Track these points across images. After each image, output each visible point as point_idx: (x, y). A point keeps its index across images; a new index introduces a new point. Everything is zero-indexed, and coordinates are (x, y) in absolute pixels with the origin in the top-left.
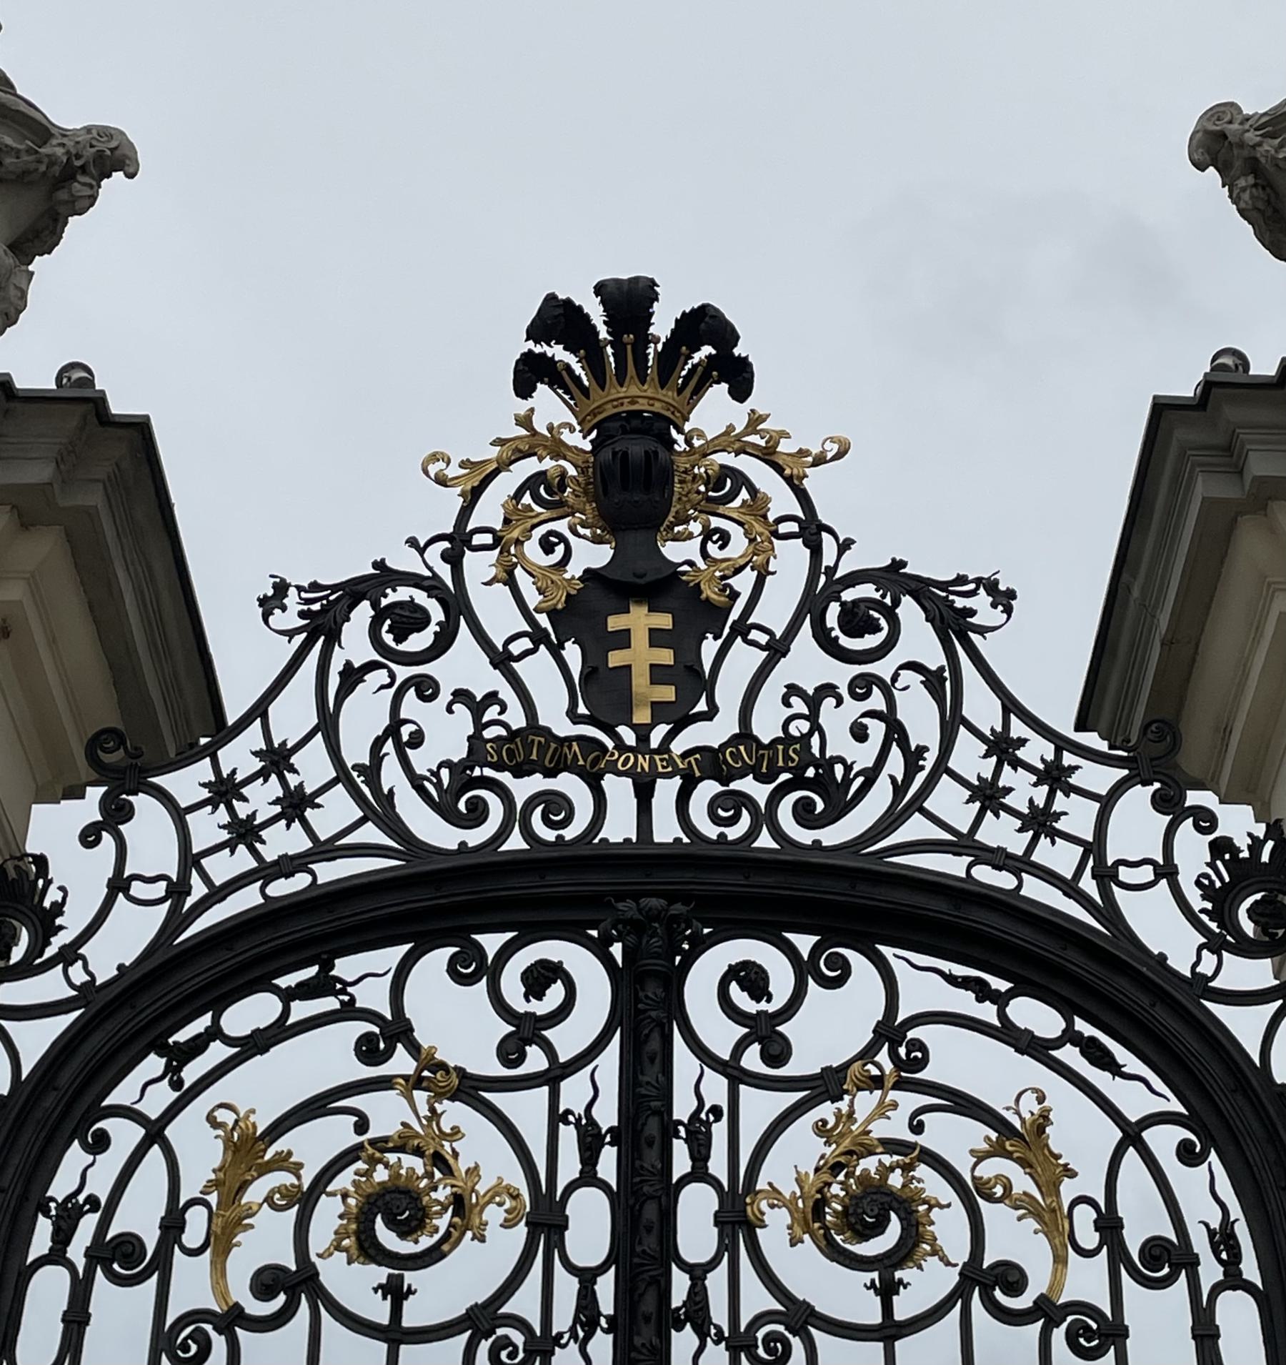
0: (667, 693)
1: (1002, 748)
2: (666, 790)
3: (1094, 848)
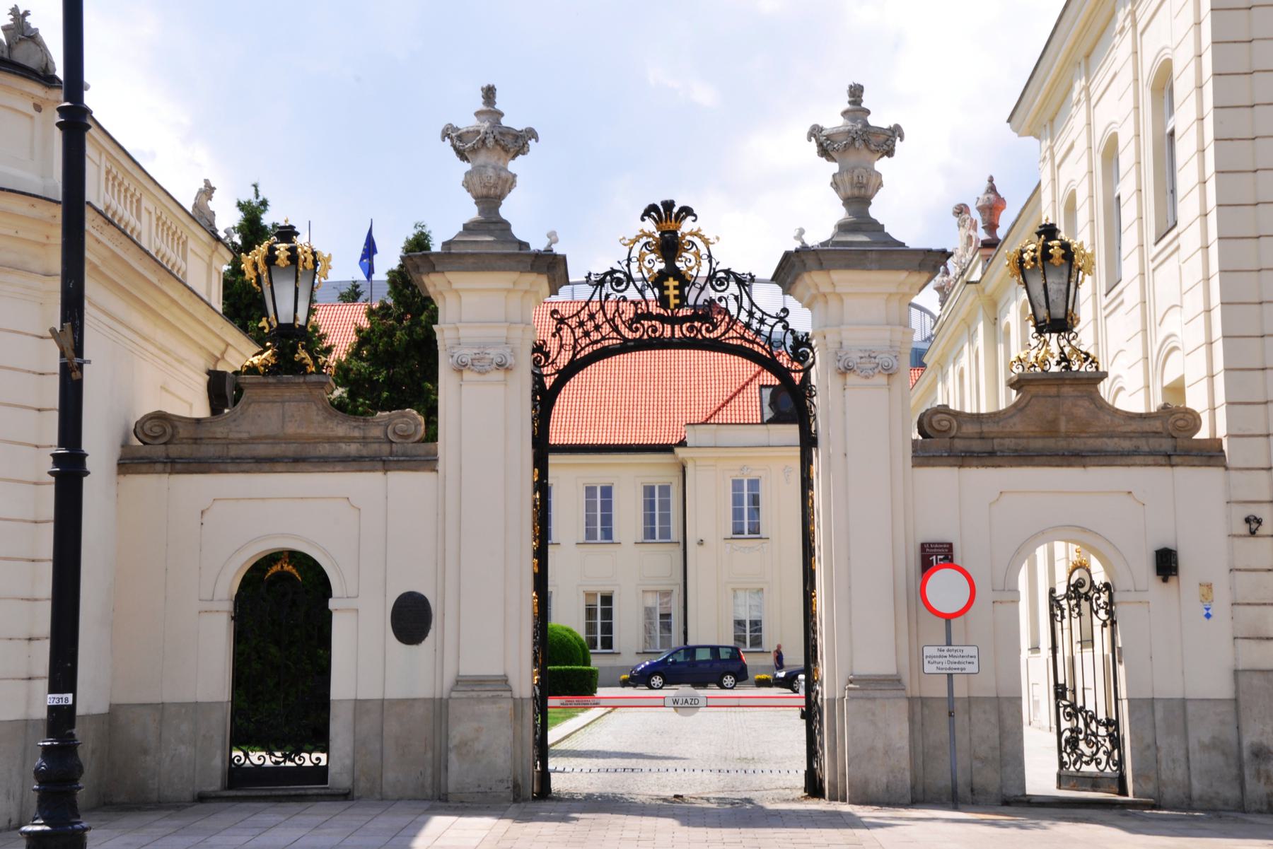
0: (677, 301)
1: (751, 314)
2: (677, 327)
3: (769, 338)
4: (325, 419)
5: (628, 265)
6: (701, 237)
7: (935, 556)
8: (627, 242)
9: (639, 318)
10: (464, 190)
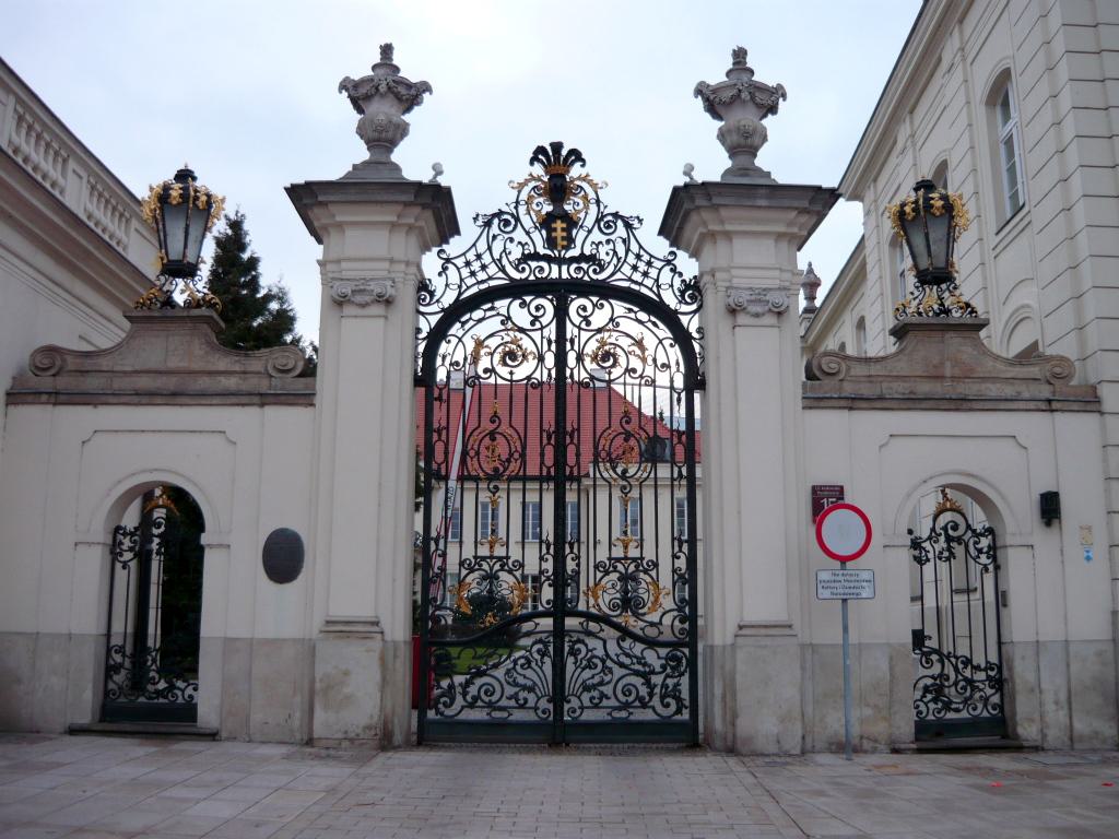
0: (565, 243)
1: (638, 257)
4: (206, 353)
5: (516, 208)
6: (590, 182)
7: (825, 501)
8: (515, 185)
9: (526, 258)
10: (358, 137)
